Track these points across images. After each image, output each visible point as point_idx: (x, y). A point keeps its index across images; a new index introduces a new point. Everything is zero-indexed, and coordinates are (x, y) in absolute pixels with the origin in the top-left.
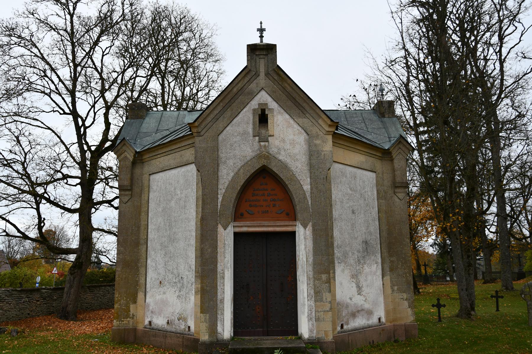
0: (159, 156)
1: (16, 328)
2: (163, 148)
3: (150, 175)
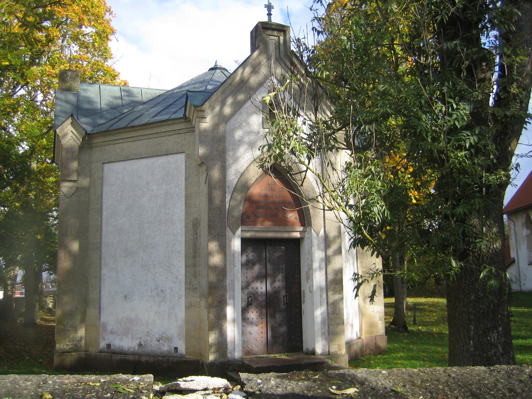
0: (121, 141)
1: (316, 265)
2: (174, 124)
3: (104, 163)
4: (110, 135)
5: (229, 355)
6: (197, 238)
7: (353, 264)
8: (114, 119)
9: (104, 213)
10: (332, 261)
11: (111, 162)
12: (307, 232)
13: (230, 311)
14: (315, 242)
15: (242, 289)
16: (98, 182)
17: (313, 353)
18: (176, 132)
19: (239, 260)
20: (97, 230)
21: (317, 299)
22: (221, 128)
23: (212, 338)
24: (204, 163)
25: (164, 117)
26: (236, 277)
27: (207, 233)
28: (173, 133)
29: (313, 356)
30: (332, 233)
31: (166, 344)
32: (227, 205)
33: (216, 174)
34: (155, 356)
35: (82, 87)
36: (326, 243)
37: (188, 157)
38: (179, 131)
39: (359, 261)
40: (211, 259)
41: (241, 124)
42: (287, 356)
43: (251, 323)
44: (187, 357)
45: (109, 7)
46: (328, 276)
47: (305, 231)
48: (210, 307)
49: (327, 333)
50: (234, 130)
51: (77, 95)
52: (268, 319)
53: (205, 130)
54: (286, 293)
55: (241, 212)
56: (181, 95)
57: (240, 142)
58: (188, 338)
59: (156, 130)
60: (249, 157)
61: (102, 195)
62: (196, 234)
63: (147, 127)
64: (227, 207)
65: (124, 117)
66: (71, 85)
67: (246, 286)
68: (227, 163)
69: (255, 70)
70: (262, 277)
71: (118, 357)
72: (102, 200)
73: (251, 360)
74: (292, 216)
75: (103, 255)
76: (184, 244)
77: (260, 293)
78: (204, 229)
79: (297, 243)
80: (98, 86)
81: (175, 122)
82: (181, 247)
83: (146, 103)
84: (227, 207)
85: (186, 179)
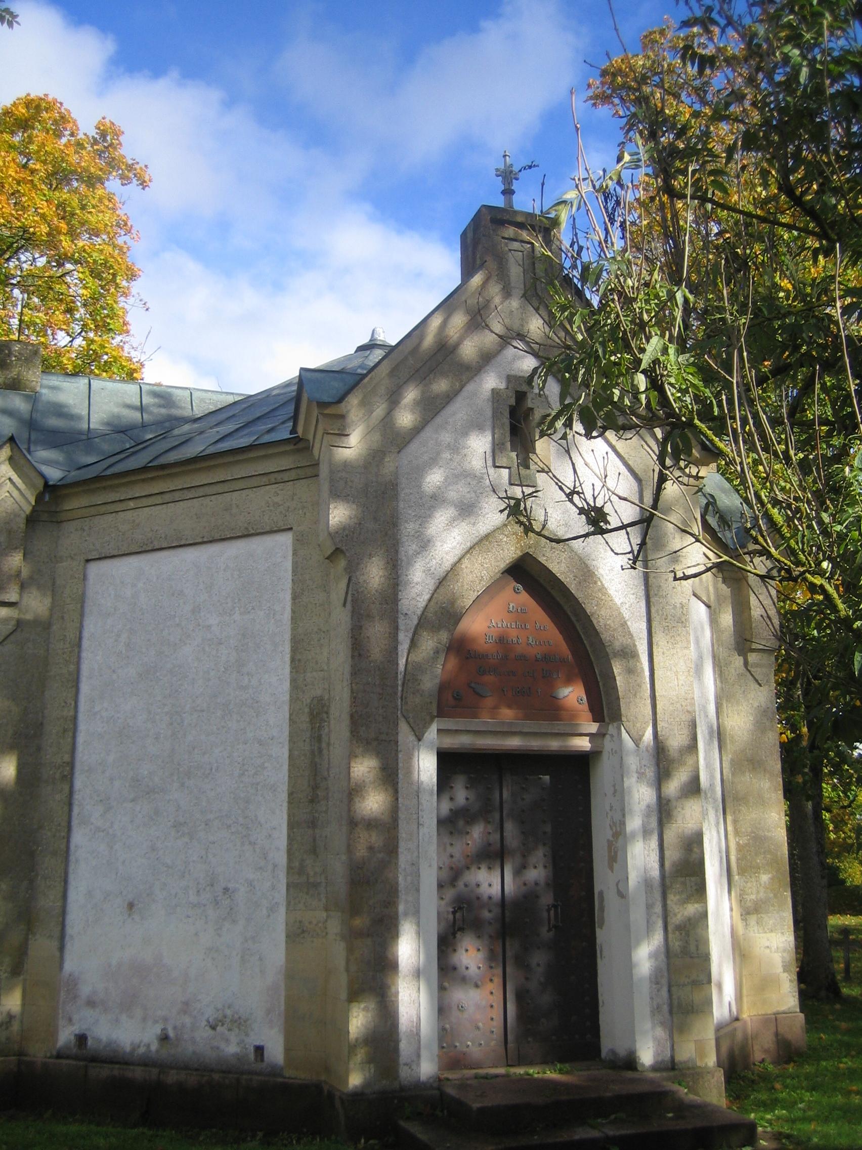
0: (132, 504)
1: (634, 823)
2: (265, 457)
3: (88, 561)
4: (105, 488)
5: (404, 1074)
6: (320, 750)
7: (718, 823)
8: (118, 453)
9: (85, 688)
10: (675, 813)
11: (106, 558)
12: (607, 736)
13: (409, 949)
14: (632, 762)
15: (440, 886)
16: (71, 609)
17: (630, 1063)
18: (272, 478)
19: (430, 808)
20: (65, 731)
21: (637, 914)
22: (389, 465)
23: (358, 1021)
24: (343, 550)
25: (242, 440)
26: (424, 858)
27: (348, 734)
28: (265, 479)
29: (630, 1074)
30: (676, 740)
31: (233, 1038)
32: (402, 662)
33: (374, 574)
34: (201, 1068)
35: (45, 382)
36: (658, 765)
37: (300, 541)
38: (279, 477)
39: (729, 818)
40: (357, 805)
41: (438, 453)
42: (561, 1071)
43: (464, 980)
44: (288, 1073)
45: (124, 218)
46: (667, 853)
47: (604, 735)
48: (352, 936)
49: (665, 1008)
50: (420, 471)
51: (34, 398)
52: (508, 970)
53: (346, 465)
54: (555, 900)
55: (437, 681)
56: (286, 400)
57: (437, 499)
58: (293, 1020)
59: (220, 475)
60: (458, 538)
61: (80, 638)
62: (319, 739)
63: (198, 466)
64: (402, 667)
65: (144, 448)
66: (18, 375)
67: (451, 878)
68: (402, 555)
69: (478, 319)
70: (493, 855)
71: (105, 1072)
72: (79, 652)
73: (463, 1086)
74: (572, 694)
75: (77, 797)
76: (286, 767)
77: (485, 897)
78: (339, 728)
79: (582, 763)
80: (86, 381)
81: (270, 451)
82: (278, 775)
83: (199, 418)
84: (402, 667)
85: (295, 597)
